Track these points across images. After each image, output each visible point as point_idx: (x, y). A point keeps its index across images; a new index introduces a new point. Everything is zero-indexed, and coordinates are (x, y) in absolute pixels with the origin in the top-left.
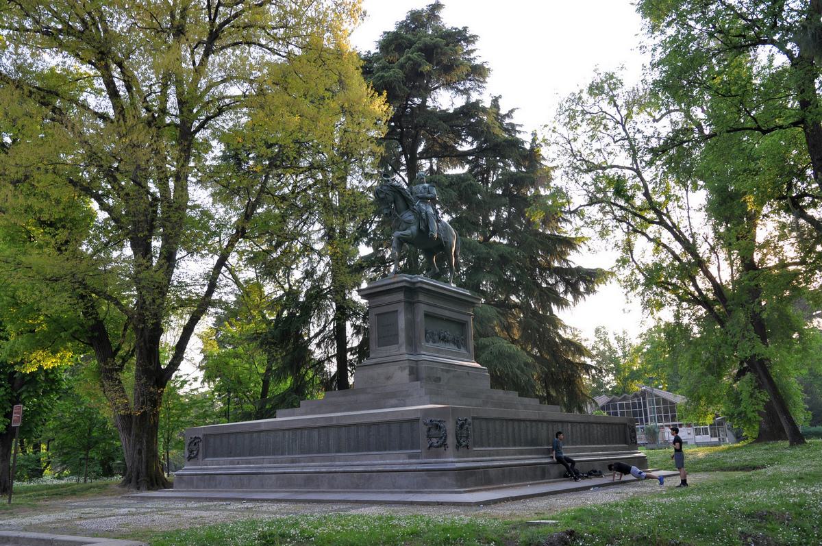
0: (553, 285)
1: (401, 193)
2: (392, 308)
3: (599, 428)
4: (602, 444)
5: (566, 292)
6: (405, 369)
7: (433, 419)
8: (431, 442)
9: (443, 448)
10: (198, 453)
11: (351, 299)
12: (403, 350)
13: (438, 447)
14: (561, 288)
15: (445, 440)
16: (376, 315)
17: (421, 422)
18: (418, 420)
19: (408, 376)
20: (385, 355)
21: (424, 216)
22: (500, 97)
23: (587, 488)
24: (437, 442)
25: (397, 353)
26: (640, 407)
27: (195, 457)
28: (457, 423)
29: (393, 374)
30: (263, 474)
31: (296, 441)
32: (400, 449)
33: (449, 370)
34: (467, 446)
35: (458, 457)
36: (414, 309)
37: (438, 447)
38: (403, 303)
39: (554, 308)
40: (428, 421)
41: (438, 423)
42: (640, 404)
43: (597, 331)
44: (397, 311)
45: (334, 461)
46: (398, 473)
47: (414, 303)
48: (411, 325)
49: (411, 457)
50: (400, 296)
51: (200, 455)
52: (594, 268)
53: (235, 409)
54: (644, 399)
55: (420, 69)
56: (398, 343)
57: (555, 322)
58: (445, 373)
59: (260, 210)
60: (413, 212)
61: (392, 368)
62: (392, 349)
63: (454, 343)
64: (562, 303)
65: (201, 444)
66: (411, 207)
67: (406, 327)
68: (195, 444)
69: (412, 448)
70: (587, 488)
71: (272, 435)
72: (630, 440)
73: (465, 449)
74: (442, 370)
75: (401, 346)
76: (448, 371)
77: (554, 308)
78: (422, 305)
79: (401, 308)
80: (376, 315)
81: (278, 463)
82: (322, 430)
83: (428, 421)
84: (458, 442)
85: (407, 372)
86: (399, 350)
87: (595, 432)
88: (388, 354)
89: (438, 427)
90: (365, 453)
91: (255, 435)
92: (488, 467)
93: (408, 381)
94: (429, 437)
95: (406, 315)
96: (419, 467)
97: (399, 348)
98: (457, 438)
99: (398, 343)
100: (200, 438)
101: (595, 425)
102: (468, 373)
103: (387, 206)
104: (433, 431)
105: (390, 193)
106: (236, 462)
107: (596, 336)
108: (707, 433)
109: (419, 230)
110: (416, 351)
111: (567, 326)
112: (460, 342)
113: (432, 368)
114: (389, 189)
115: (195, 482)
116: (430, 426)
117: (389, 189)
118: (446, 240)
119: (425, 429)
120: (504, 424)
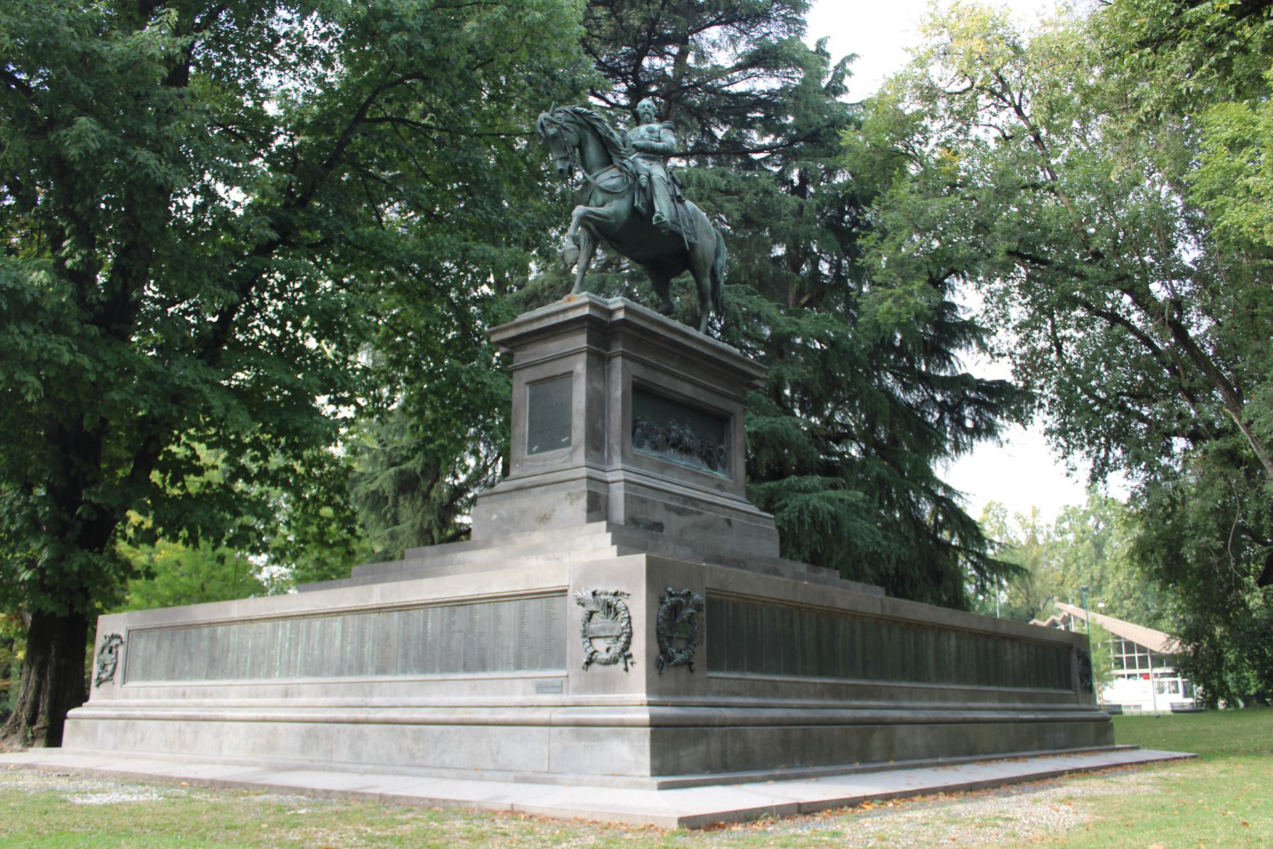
2: (559, 368)
3: (1016, 651)
4: (1023, 685)
6: (578, 497)
7: (600, 589)
8: (590, 650)
9: (621, 665)
10: (115, 667)
12: (580, 457)
13: (607, 663)
15: (628, 643)
16: (527, 383)
17: (570, 599)
18: (563, 592)
20: (540, 470)
24: (608, 650)
25: (568, 465)
27: (107, 680)
28: (662, 602)
29: (553, 510)
30: (224, 720)
31: (297, 644)
32: (519, 667)
34: (689, 664)
36: (609, 370)
37: (607, 663)
38: (584, 356)
40: (587, 594)
41: (610, 598)
45: (371, 694)
46: (337, 726)
48: (597, 406)
49: (541, 688)
50: (581, 341)
51: (118, 676)
52: (988, 379)
56: (568, 444)
60: (621, 170)
62: (554, 458)
63: (700, 455)
65: (121, 650)
66: (616, 161)
68: (110, 652)
69: (546, 665)
71: (251, 632)
73: (684, 671)
74: (668, 507)
75: (574, 450)
76: (680, 512)
79: (580, 366)
80: (527, 383)
81: (258, 696)
82: (349, 618)
83: (587, 594)
84: (663, 651)
86: (571, 459)
87: (1008, 657)
88: (547, 469)
89: (610, 609)
90: (439, 677)
91: (220, 629)
92: (744, 723)
94: (589, 637)
96: (558, 715)
97: (571, 453)
99: (568, 444)
100: (119, 637)
102: (729, 522)
104: (599, 621)
105: (570, 127)
106: (180, 690)
108: (1176, 691)
109: (634, 210)
112: (713, 458)
113: (644, 501)
114: (569, 118)
115: (99, 734)
116: (593, 608)
117: (569, 118)
118: (693, 240)
119: (579, 613)
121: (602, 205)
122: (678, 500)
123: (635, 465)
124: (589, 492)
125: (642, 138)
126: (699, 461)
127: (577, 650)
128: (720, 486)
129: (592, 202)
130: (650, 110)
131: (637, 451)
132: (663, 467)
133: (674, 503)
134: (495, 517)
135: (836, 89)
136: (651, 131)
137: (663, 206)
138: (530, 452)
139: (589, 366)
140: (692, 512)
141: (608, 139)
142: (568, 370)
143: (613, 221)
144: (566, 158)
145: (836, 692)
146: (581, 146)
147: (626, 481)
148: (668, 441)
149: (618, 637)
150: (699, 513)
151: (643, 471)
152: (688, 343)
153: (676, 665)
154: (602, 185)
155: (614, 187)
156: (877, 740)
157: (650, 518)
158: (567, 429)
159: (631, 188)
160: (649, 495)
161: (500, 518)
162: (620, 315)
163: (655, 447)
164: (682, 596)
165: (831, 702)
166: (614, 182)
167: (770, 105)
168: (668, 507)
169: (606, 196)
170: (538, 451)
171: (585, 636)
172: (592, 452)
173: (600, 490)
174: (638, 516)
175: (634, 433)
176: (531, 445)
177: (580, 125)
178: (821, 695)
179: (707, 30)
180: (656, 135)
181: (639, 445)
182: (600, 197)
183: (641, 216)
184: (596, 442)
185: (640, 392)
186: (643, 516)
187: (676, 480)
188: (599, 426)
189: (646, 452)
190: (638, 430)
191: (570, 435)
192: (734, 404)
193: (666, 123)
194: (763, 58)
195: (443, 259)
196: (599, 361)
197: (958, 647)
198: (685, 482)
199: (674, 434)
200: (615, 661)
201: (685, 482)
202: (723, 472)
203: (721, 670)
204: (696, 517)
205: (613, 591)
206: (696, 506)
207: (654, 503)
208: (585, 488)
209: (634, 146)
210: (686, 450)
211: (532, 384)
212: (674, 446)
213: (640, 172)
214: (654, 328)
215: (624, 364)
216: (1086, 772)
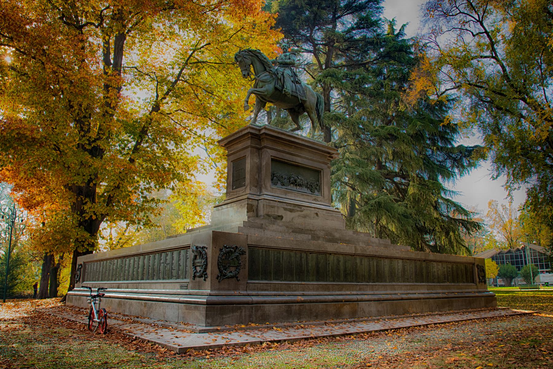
0: (442, 161)
1: (257, 56)
2: (242, 154)
5: (452, 167)
6: (244, 207)
14: (448, 164)
22: (407, 24)
26: (521, 258)
33: (293, 210)
34: (235, 277)
35: (219, 289)
39: (440, 178)
42: (521, 255)
43: (490, 204)
47: (261, 149)
54: (524, 252)
55: (533, 180)
57: (440, 188)
60: (269, 73)
63: (307, 187)
64: (448, 175)
66: (268, 69)
72: (478, 280)
75: (246, 187)
76: (291, 211)
77: (440, 178)
78: (268, 150)
79: (248, 152)
80: (232, 161)
86: (245, 191)
97: (245, 189)
98: (219, 268)
101: (435, 264)
103: (245, 68)
107: (489, 208)
109: (276, 89)
111: (447, 190)
117: (247, 53)
120: (371, 259)
122: (290, 206)
127: (190, 270)
131: (274, 187)
133: (289, 207)
135: (400, 34)
139: (251, 152)
140: (298, 211)
142: (244, 155)
143: (266, 93)
144: (246, 70)
145: (327, 288)
147: (248, 198)
149: (203, 266)
150: (302, 211)
151: (276, 195)
153: (228, 278)
155: (266, 80)
156: (347, 308)
157: (276, 214)
164: (233, 248)
165: (322, 293)
166: (266, 78)
168: (285, 209)
170: (236, 188)
171: (193, 266)
172: (254, 188)
174: (270, 213)
175: (272, 180)
176: (233, 186)
177: (251, 56)
178: (317, 290)
180: (288, 57)
186: (273, 213)
190: (275, 178)
192: (323, 165)
197: (404, 267)
200: (202, 277)
203: (258, 279)
204: (300, 213)
205: (201, 247)
207: (278, 207)
211: (274, 160)
214: (280, 136)
216: (359, 335)
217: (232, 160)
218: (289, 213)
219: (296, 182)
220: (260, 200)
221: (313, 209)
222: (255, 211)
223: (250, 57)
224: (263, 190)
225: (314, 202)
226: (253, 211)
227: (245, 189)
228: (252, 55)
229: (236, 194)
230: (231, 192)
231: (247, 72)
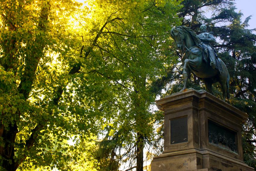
2: (182, 114)
6: (194, 159)
11: (151, 127)
12: (191, 145)
16: (170, 119)
19: (196, 165)
20: (176, 150)
21: (206, 51)
23: (232, 128)
38: (192, 110)
44: (187, 115)
48: (197, 127)
53: (89, 105)
56: (186, 140)
58: (225, 167)
59: (16, 8)
61: (184, 159)
66: (197, 44)
67: (194, 128)
70: (232, 128)
75: (189, 143)
76: (226, 166)
79: (190, 113)
85: (195, 162)
86: (188, 146)
88: (179, 149)
93: (196, 169)
95: (194, 118)
97: (188, 144)
99: (186, 140)
109: (203, 60)
110: (201, 147)
113: (215, 161)
117: (182, 30)
121: (193, 59)
122: (225, 161)
123: (210, 149)
124: (197, 157)
125: (203, 37)
126: (228, 148)
128: (236, 157)
129: (189, 58)
130: (205, 28)
132: (219, 150)
133: (224, 162)
134: (160, 166)
136: (206, 35)
137: (213, 59)
138: (171, 143)
139: (193, 113)
140: (230, 166)
141: (194, 37)
142: (186, 115)
146: (185, 40)
147: (196, 152)
148: (219, 140)
150: (232, 167)
152: (225, 106)
154: (193, 52)
155: (197, 53)
157: (217, 168)
158: (186, 135)
159: (202, 53)
160: (216, 159)
161: (162, 166)
162: (204, 96)
163: (215, 143)
167: (222, 32)
168: (223, 164)
169: (195, 56)
170: (174, 143)
172: (195, 143)
173: (201, 157)
174: (214, 167)
175: (209, 137)
177: (185, 32)
179: (202, 7)
180: (208, 36)
181: (210, 142)
182: (192, 56)
183: (206, 63)
184: (196, 140)
185: (211, 123)
187: (223, 154)
188: (197, 134)
189: (212, 143)
191: (187, 137)
193: (211, 32)
194: (224, 15)
195: (246, 83)
196: (196, 111)
198: (225, 155)
199: (220, 138)
201: (225, 155)
202: (236, 152)
206: (231, 164)
208: (195, 156)
209: (201, 40)
210: (224, 144)
212: (221, 142)
213: (205, 48)
215: (205, 113)
217: (171, 118)
218: (225, 167)
219: (223, 141)
220: (204, 154)
221: (238, 165)
222: (201, 164)
223: (184, 33)
224: (203, 146)
225: (235, 159)
226: (201, 164)
227: (188, 144)
228: (186, 31)
229: (177, 148)
230: (170, 146)
231: (181, 45)
